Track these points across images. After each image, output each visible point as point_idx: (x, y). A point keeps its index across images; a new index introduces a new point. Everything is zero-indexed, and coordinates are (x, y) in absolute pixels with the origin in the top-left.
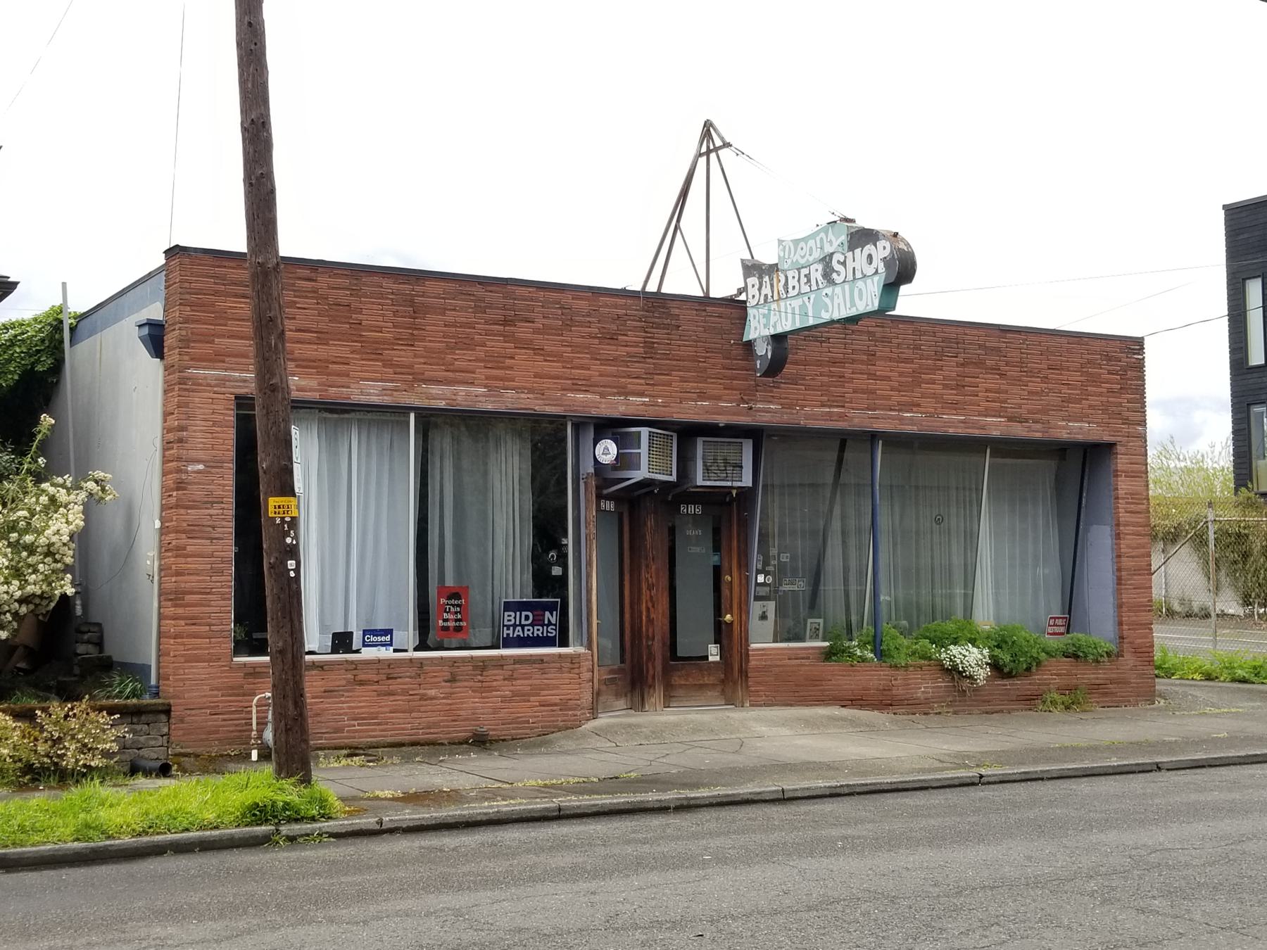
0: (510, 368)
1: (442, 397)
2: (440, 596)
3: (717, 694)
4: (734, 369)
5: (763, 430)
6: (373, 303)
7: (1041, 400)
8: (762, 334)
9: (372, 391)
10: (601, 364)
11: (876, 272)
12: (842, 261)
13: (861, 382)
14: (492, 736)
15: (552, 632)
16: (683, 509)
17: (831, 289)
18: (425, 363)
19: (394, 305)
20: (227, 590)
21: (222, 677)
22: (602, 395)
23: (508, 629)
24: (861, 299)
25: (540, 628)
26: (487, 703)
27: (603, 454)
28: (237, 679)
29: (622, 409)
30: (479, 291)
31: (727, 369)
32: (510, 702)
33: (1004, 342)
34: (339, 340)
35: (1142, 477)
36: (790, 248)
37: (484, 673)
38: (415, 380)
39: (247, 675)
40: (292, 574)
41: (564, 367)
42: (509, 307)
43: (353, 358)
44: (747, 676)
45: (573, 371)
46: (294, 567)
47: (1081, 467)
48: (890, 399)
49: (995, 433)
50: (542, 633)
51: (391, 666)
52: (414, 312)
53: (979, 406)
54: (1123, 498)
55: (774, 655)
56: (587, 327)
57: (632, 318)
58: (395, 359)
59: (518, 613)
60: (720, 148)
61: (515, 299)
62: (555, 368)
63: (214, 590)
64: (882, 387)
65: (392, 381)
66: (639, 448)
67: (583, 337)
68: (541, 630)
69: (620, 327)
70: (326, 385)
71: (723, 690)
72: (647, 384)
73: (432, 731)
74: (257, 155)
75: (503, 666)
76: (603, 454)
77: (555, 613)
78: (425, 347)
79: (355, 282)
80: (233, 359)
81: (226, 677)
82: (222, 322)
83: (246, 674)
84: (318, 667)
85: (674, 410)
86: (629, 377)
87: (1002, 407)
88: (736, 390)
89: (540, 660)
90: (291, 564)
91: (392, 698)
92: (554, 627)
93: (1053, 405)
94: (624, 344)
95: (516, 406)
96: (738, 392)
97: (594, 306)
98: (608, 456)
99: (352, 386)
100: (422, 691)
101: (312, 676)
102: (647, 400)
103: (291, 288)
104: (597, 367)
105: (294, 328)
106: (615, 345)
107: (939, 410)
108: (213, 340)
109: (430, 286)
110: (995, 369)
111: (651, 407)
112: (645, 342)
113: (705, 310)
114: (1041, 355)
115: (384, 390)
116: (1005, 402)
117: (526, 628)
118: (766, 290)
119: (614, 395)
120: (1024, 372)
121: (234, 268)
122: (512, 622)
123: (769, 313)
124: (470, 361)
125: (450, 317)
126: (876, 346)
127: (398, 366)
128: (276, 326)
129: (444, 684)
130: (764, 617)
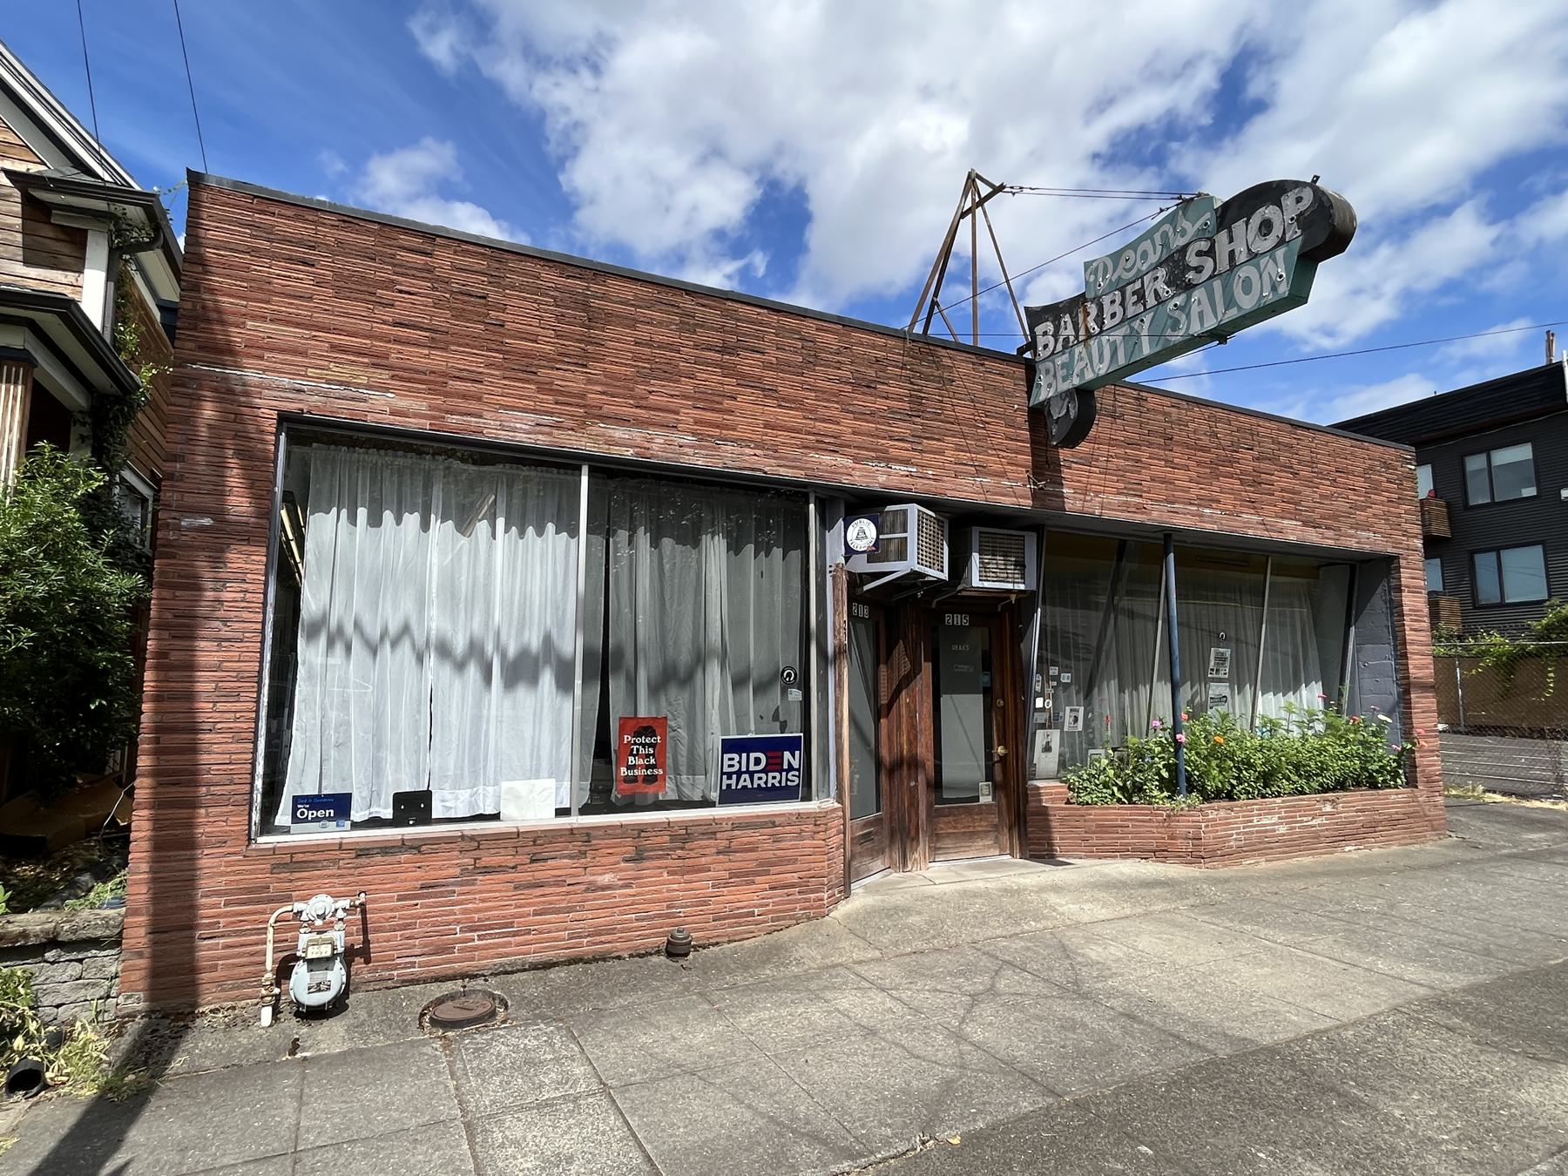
2: (622, 732)
4: (1019, 441)
8: (1059, 390)
9: (518, 425)
10: (855, 419)
11: (1282, 242)
13: (1159, 469)
14: (698, 939)
15: (794, 779)
16: (948, 619)
17: (1183, 296)
18: (603, 393)
21: (227, 874)
22: (856, 460)
23: (729, 778)
25: (777, 774)
27: (857, 538)
28: (260, 875)
29: (882, 479)
30: (687, 303)
34: (467, 345)
37: (687, 846)
39: (276, 868)
41: (805, 418)
44: (1025, 822)
45: (817, 424)
47: (1348, 581)
48: (1188, 492)
49: (1292, 538)
50: (780, 782)
56: (835, 368)
59: (744, 755)
61: (738, 320)
63: (219, 726)
65: (552, 414)
66: (905, 531)
68: (778, 779)
70: (440, 410)
71: (996, 837)
72: (914, 450)
73: (603, 938)
76: (857, 538)
77: (797, 753)
80: (280, 356)
85: (948, 485)
86: (891, 438)
88: (1021, 466)
89: (770, 822)
91: (539, 891)
92: (797, 773)
94: (885, 395)
95: (737, 464)
99: (487, 415)
100: (591, 878)
101: (400, 863)
102: (914, 470)
107: (1239, 509)
109: (614, 286)
110: (1287, 468)
113: (983, 365)
117: (756, 776)
119: (872, 459)
121: (288, 217)
122: (736, 769)
124: (672, 396)
125: (643, 332)
126: (1173, 429)
127: (561, 393)
130: (1047, 749)
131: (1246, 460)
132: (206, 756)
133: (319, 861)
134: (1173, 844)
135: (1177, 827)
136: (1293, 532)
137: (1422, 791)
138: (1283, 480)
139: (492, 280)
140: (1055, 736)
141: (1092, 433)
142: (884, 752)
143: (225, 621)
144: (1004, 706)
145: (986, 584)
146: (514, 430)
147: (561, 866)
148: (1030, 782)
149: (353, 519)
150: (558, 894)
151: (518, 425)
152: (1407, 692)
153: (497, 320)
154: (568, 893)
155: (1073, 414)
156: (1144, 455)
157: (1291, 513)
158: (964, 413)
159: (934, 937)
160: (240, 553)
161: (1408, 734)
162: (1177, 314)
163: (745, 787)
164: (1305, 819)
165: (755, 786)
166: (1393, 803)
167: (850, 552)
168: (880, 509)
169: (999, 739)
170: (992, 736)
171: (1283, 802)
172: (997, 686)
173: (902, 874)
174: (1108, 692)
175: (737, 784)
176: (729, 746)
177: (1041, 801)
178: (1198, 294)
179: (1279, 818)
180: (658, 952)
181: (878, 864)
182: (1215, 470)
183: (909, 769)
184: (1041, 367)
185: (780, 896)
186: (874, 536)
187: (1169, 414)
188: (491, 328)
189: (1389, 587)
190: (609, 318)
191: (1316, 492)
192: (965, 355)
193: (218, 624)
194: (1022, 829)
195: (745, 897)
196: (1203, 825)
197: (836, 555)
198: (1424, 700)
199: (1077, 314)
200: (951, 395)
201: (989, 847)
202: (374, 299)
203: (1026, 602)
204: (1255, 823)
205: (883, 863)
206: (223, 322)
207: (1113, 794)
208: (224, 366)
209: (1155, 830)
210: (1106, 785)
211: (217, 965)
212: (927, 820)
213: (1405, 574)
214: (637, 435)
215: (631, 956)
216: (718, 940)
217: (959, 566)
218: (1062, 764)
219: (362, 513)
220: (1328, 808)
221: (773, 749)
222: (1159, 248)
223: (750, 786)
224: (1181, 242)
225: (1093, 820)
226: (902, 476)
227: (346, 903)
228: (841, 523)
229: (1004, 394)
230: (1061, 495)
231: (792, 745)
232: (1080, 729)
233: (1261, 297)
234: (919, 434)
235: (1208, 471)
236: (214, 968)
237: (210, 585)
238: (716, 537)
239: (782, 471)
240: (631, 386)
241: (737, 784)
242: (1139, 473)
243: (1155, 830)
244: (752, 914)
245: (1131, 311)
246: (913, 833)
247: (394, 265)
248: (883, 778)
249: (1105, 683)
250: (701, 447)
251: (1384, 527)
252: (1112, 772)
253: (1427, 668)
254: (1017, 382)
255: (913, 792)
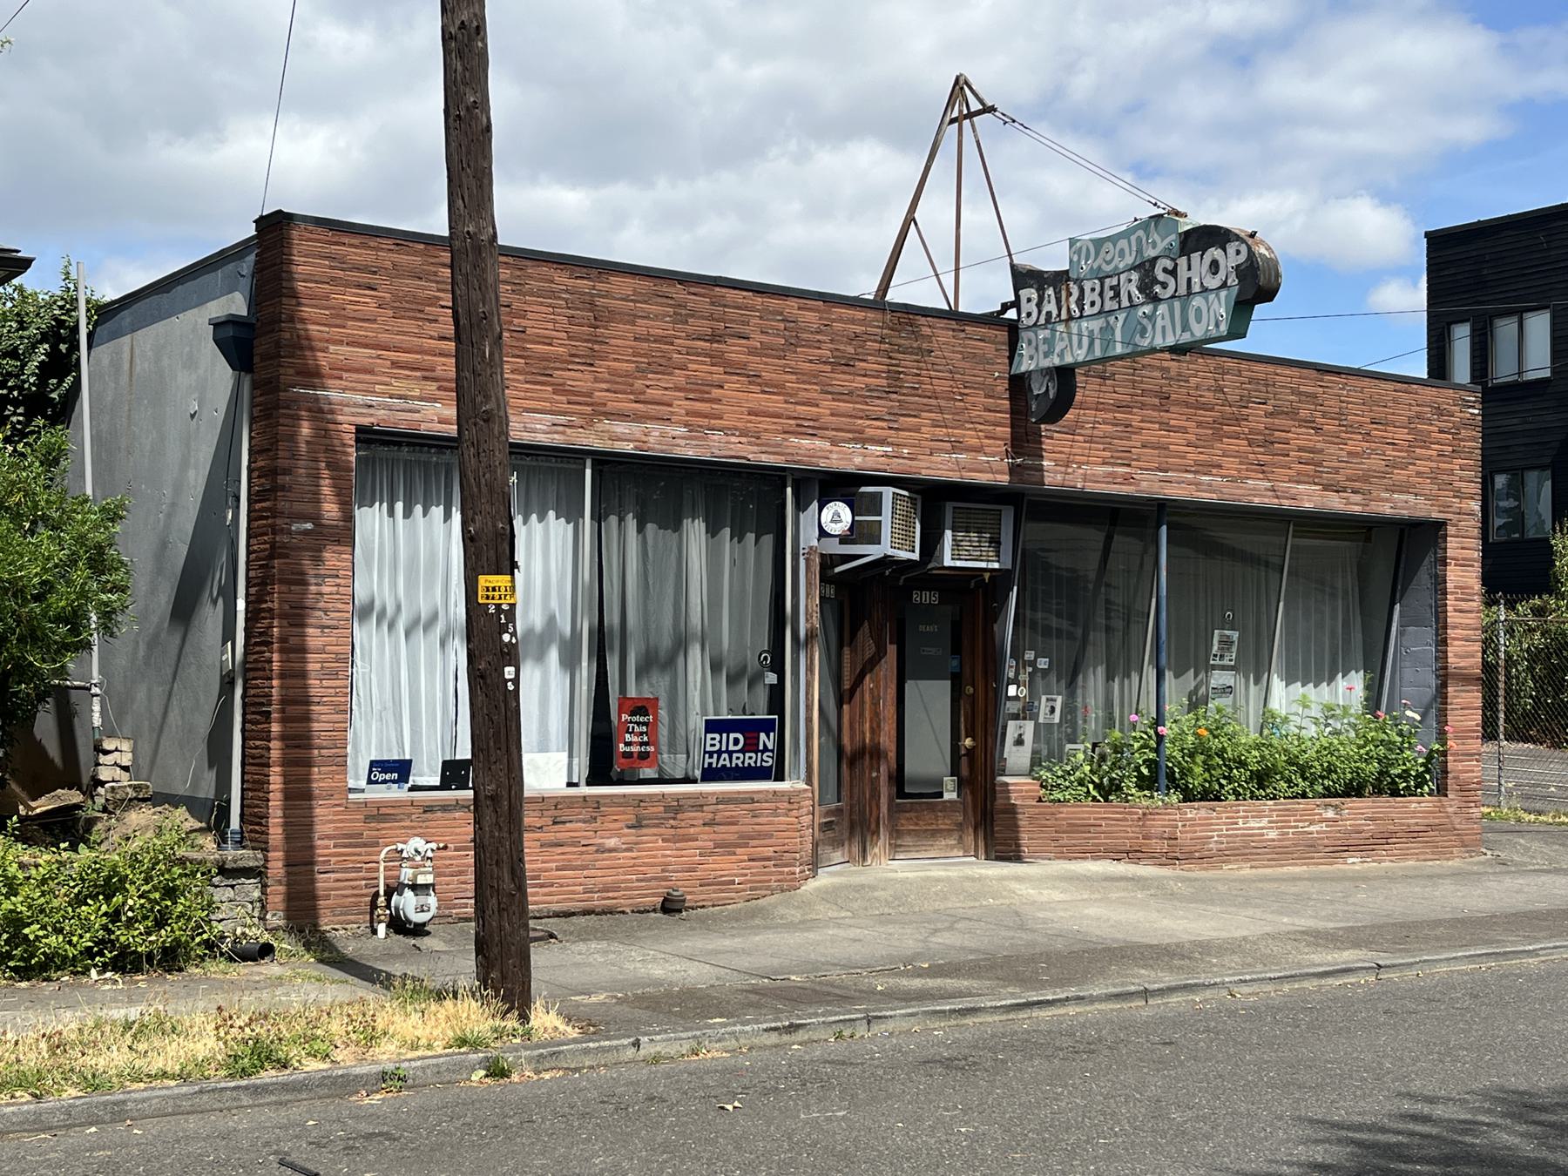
0: (718, 401)
1: (628, 437)
3: (953, 842)
5: (1023, 495)
6: (541, 304)
7: (1362, 463)
9: (538, 426)
10: (834, 400)
11: (1224, 285)
12: (1170, 268)
13: (1153, 433)
15: (770, 762)
18: (607, 391)
19: (569, 308)
20: (343, 699)
22: (834, 443)
23: (711, 757)
24: (1199, 322)
25: (753, 755)
26: (682, 856)
27: (832, 521)
29: (858, 460)
30: (678, 292)
31: (990, 411)
32: (711, 854)
33: (1321, 386)
35: (1473, 566)
36: (1088, 250)
37: (679, 816)
38: (596, 413)
39: (369, 818)
40: (511, 686)
41: (786, 402)
42: (717, 316)
43: (514, 380)
44: (992, 820)
45: (798, 407)
46: (513, 677)
48: (1184, 458)
49: (1308, 505)
50: (756, 762)
51: (559, 807)
52: (595, 318)
53: (1290, 468)
54: (1452, 593)
55: (1026, 792)
57: (872, 337)
58: (569, 383)
59: (725, 735)
60: (978, 113)
61: (725, 306)
62: (775, 403)
63: (325, 699)
64: (1176, 441)
65: (564, 414)
66: (881, 515)
67: (811, 361)
68: (754, 759)
69: (860, 350)
71: (961, 837)
72: (890, 428)
73: (610, 895)
74: (467, 74)
75: (702, 806)
76: (832, 521)
77: (772, 734)
78: (608, 368)
79: (518, 273)
81: (342, 821)
82: (338, 322)
83: (367, 817)
84: (464, 807)
86: (868, 418)
87: (1316, 471)
89: (750, 799)
90: (509, 672)
91: (560, 850)
92: (771, 754)
93: (1375, 471)
94: (863, 372)
96: (1002, 443)
97: (826, 319)
98: (839, 525)
101: (455, 819)
102: (890, 449)
103: (432, 278)
104: (827, 404)
105: (436, 334)
106: (850, 374)
107: (1244, 474)
108: (327, 348)
110: (1309, 423)
111: (895, 459)
112: (889, 371)
113: (963, 331)
114: (1363, 404)
115: (554, 425)
116: (1320, 465)
117: (735, 755)
118: (1051, 307)
119: (849, 441)
120: (1343, 426)
121: (356, 247)
123: (1053, 336)
124: (666, 389)
125: (642, 327)
126: (1171, 386)
128: (491, 325)
129: (626, 831)
131: (1257, 417)
132: (316, 724)
133: (397, 815)
134: (1146, 845)
135: (1153, 826)
136: (1310, 498)
137: (1452, 801)
138: (1301, 437)
139: (514, 288)
140: (1029, 727)
141: (1078, 398)
142: (846, 740)
143: (326, 611)
144: (973, 694)
145: (959, 564)
146: (534, 431)
147: (576, 829)
148: (999, 778)
149: (391, 513)
150: (574, 853)
151: (538, 426)
152: (1444, 685)
153: (519, 326)
154: (582, 853)
155: (1052, 394)
156: (1135, 420)
157: (1308, 475)
158: (942, 386)
159: (899, 906)
160: (333, 552)
161: (1442, 736)
162: (1145, 322)
163: (724, 766)
164: (1301, 824)
165: (734, 765)
166: (1414, 812)
167: (823, 533)
168: (853, 490)
169: (966, 731)
170: (959, 722)
171: (1275, 804)
172: (967, 671)
173: (861, 867)
174: (1094, 681)
175: (717, 764)
176: (712, 726)
177: (1009, 798)
178: (1162, 309)
179: (1270, 822)
180: (654, 911)
181: (838, 856)
182: (1217, 430)
183: (871, 758)
184: (1024, 335)
185: (757, 867)
186: (850, 520)
187: (1166, 370)
188: (514, 334)
189: (1435, 558)
190: (612, 316)
191: (1342, 449)
192: (946, 321)
193: (321, 613)
194: (988, 827)
195: (723, 866)
196: (1180, 824)
197: (810, 538)
198: (1463, 694)
199: (1060, 291)
200: (930, 366)
201: (952, 847)
202: (422, 316)
203: (1000, 581)
204: (1241, 825)
205: (843, 855)
206: (312, 349)
207: (1088, 792)
208: (314, 387)
209: (1129, 829)
210: (1081, 783)
211: (330, 895)
212: (889, 815)
213: (1452, 543)
214: (635, 429)
215: (633, 911)
216: (704, 903)
217: (930, 544)
218: (1036, 761)
219: (399, 506)
220: (1330, 814)
221: (751, 729)
222: (1134, 254)
223: (728, 765)
224: (1151, 253)
225: (1064, 819)
226: (877, 456)
227: (434, 846)
228: (815, 505)
229: (984, 360)
230: (1041, 469)
231: (767, 726)
232: (1057, 720)
233: (1207, 330)
234: (896, 411)
235: (1211, 432)
236: (327, 897)
237: (313, 581)
238: (697, 521)
239: (764, 457)
240: (631, 381)
241: (717, 764)
242: (1129, 439)
243: (1129, 829)
244: (733, 882)
245: (1109, 305)
246: (873, 826)
247: (437, 282)
248: (844, 766)
249: (1091, 669)
250: (691, 438)
251: (1428, 486)
252: (1089, 768)
253: (1473, 657)
254: (999, 347)
255: (874, 784)
